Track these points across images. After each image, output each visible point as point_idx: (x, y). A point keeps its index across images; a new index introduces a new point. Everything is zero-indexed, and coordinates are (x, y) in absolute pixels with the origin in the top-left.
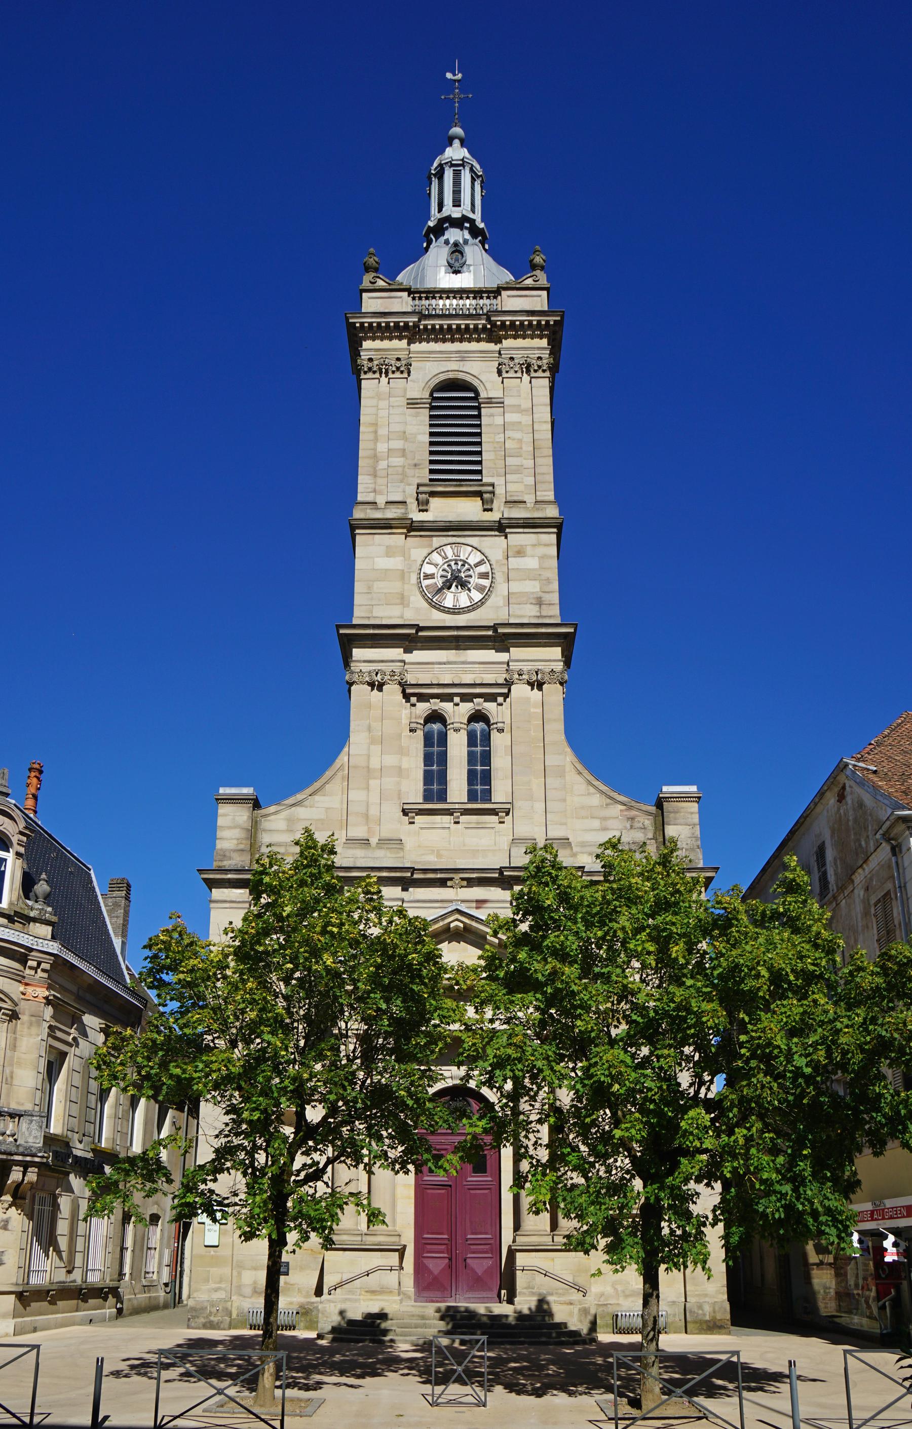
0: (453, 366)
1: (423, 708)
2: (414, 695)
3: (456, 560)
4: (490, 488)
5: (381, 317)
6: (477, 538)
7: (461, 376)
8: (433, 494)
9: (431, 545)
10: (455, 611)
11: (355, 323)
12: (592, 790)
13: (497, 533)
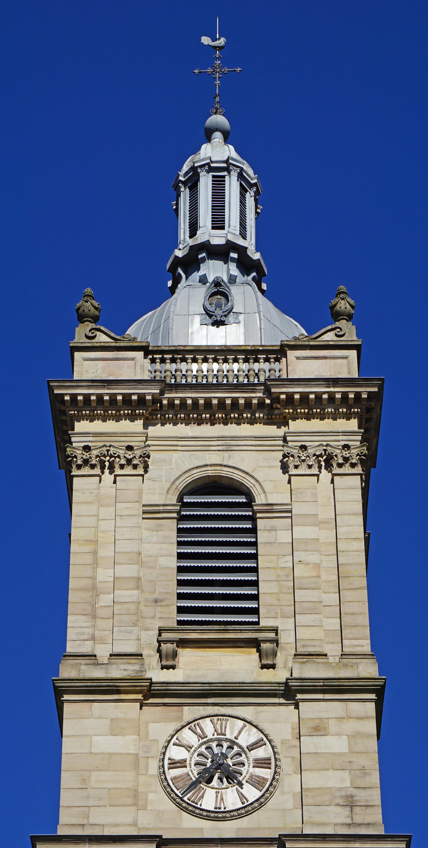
0: (214, 458)
3: (219, 740)
4: (272, 635)
5: (104, 387)
6: (251, 708)
7: (226, 472)
8: (183, 643)
9: (180, 718)
11: (63, 395)
13: (282, 701)
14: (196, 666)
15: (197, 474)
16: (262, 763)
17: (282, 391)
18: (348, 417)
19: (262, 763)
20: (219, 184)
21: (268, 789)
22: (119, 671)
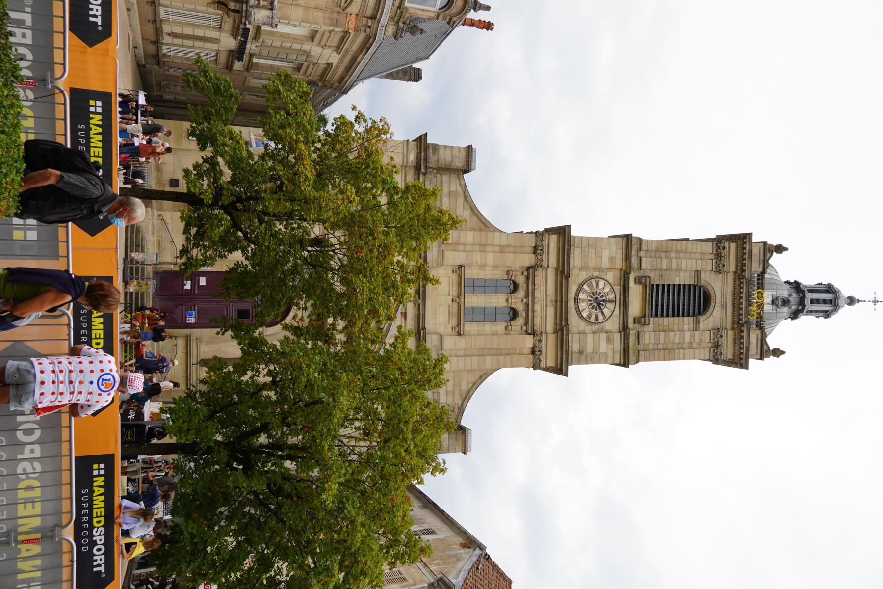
1: (521, 280)
2: (529, 274)
7: (712, 305)
10: (577, 300)
12: (470, 385)
14: (636, 292)
15: (712, 293)
16: (597, 318)
17: (744, 329)
18: (734, 355)
19: (597, 318)
20: (829, 302)
21: (587, 320)
22: (634, 260)
